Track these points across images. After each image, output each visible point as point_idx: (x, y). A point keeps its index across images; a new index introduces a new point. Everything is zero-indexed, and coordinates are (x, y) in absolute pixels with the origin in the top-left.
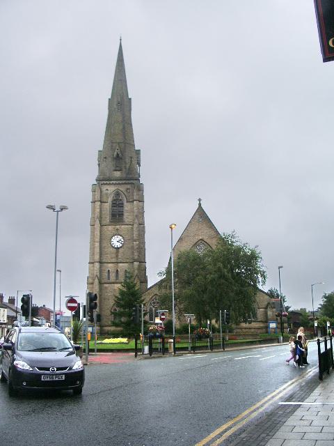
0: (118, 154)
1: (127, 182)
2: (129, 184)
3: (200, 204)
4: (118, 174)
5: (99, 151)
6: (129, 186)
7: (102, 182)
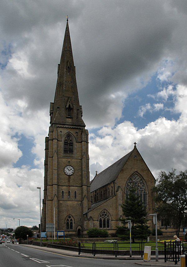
0: (69, 106)
1: (76, 127)
3: (135, 146)
4: (69, 120)
6: (77, 131)
7: (58, 126)
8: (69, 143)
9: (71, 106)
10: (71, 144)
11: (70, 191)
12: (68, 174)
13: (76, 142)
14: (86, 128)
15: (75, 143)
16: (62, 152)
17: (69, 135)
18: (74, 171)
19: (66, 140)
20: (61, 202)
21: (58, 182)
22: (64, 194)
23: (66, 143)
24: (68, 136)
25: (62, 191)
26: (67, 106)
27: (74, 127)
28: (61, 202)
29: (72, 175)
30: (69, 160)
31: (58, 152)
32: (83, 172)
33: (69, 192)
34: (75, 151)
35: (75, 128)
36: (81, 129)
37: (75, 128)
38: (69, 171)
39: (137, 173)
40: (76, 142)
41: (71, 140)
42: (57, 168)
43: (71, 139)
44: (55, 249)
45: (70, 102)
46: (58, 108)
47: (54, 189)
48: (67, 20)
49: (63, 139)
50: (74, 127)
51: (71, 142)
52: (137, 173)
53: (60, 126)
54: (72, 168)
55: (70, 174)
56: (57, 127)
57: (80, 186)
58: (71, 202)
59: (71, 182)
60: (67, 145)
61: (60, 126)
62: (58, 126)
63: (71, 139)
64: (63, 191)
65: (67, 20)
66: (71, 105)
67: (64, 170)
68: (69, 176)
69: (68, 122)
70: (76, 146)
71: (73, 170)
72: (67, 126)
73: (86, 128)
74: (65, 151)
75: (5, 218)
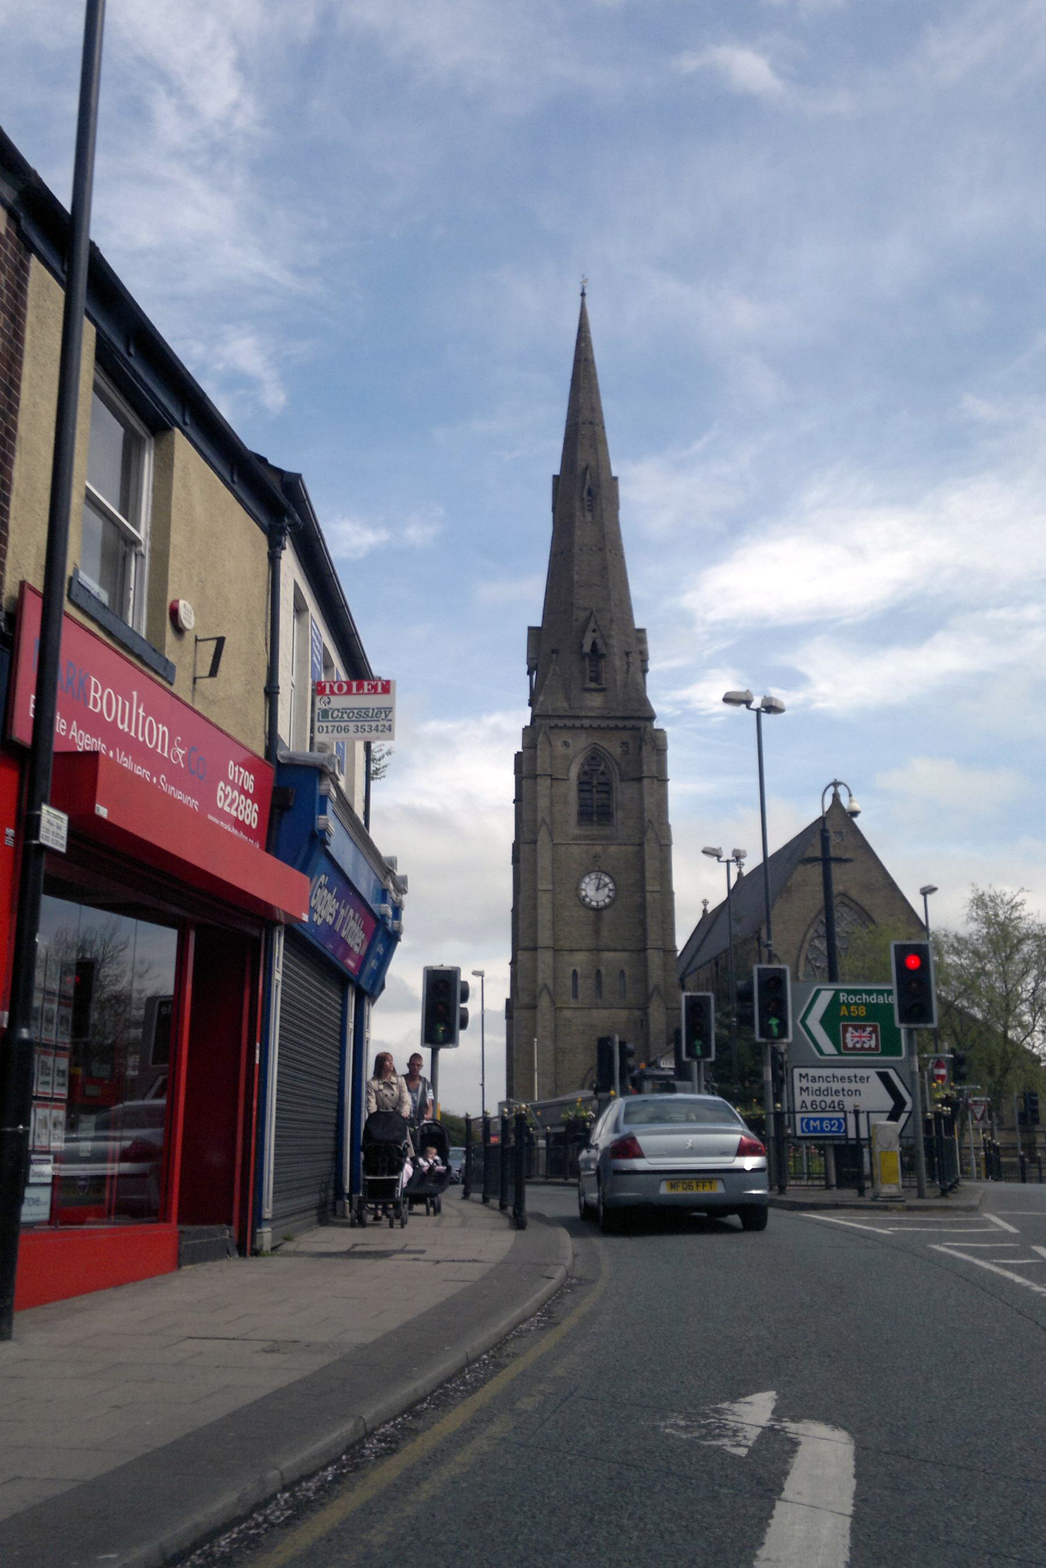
0: (594, 644)
1: (621, 724)
2: (625, 728)
3: (836, 797)
4: (595, 702)
5: (555, 477)
6: (625, 736)
7: (553, 722)
8: (595, 782)
9: (602, 649)
10: (607, 788)
11: (603, 970)
12: (594, 904)
13: (622, 780)
14: (656, 725)
15: (617, 784)
16: (573, 818)
17: (595, 757)
18: (616, 890)
19: (585, 773)
20: (567, 1013)
21: (555, 937)
22: (580, 982)
23: (584, 785)
24: (593, 758)
25: (572, 969)
26: (587, 648)
27: (612, 723)
28: (567, 1013)
29: (607, 907)
30: (599, 848)
31: (553, 822)
32: (648, 895)
33: (599, 972)
34: (619, 815)
35: (616, 728)
36: (638, 729)
37: (616, 728)
38: (594, 891)
39: (847, 901)
40: (622, 780)
41: (603, 773)
42: (553, 883)
43: (602, 768)
44: (356, 773)
45: (594, 631)
46: (553, 652)
47: (541, 966)
48: (583, 295)
49: (574, 771)
50: (612, 723)
51: (603, 779)
52: (847, 901)
53: (561, 723)
54: (607, 880)
55: (602, 904)
56: (551, 728)
57: (639, 951)
58: (605, 1013)
59: (604, 933)
60: (591, 791)
61: (561, 723)
62: (553, 722)
63: (602, 768)
64: (575, 972)
65: (583, 295)
66: (599, 642)
67: (580, 881)
68: (598, 910)
69: (591, 709)
70: (623, 793)
71: (611, 886)
72: (586, 723)
73: (656, 725)
74: (585, 815)
75: (94, 1016)
